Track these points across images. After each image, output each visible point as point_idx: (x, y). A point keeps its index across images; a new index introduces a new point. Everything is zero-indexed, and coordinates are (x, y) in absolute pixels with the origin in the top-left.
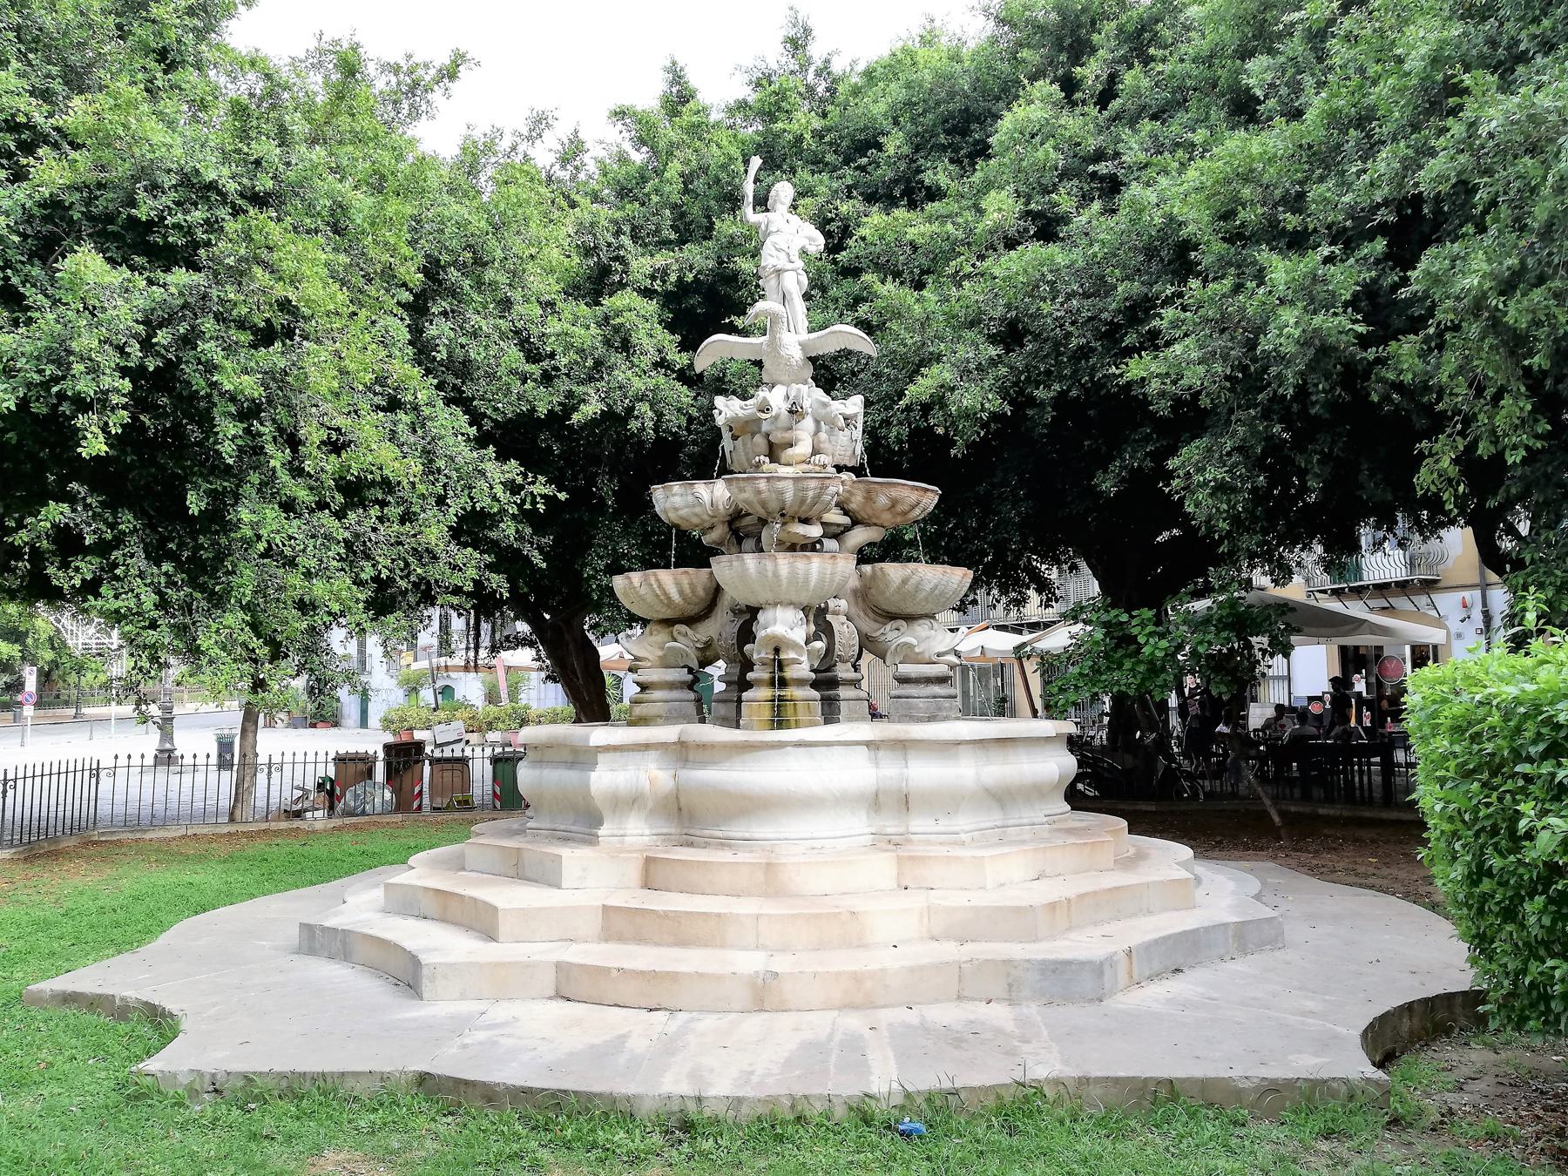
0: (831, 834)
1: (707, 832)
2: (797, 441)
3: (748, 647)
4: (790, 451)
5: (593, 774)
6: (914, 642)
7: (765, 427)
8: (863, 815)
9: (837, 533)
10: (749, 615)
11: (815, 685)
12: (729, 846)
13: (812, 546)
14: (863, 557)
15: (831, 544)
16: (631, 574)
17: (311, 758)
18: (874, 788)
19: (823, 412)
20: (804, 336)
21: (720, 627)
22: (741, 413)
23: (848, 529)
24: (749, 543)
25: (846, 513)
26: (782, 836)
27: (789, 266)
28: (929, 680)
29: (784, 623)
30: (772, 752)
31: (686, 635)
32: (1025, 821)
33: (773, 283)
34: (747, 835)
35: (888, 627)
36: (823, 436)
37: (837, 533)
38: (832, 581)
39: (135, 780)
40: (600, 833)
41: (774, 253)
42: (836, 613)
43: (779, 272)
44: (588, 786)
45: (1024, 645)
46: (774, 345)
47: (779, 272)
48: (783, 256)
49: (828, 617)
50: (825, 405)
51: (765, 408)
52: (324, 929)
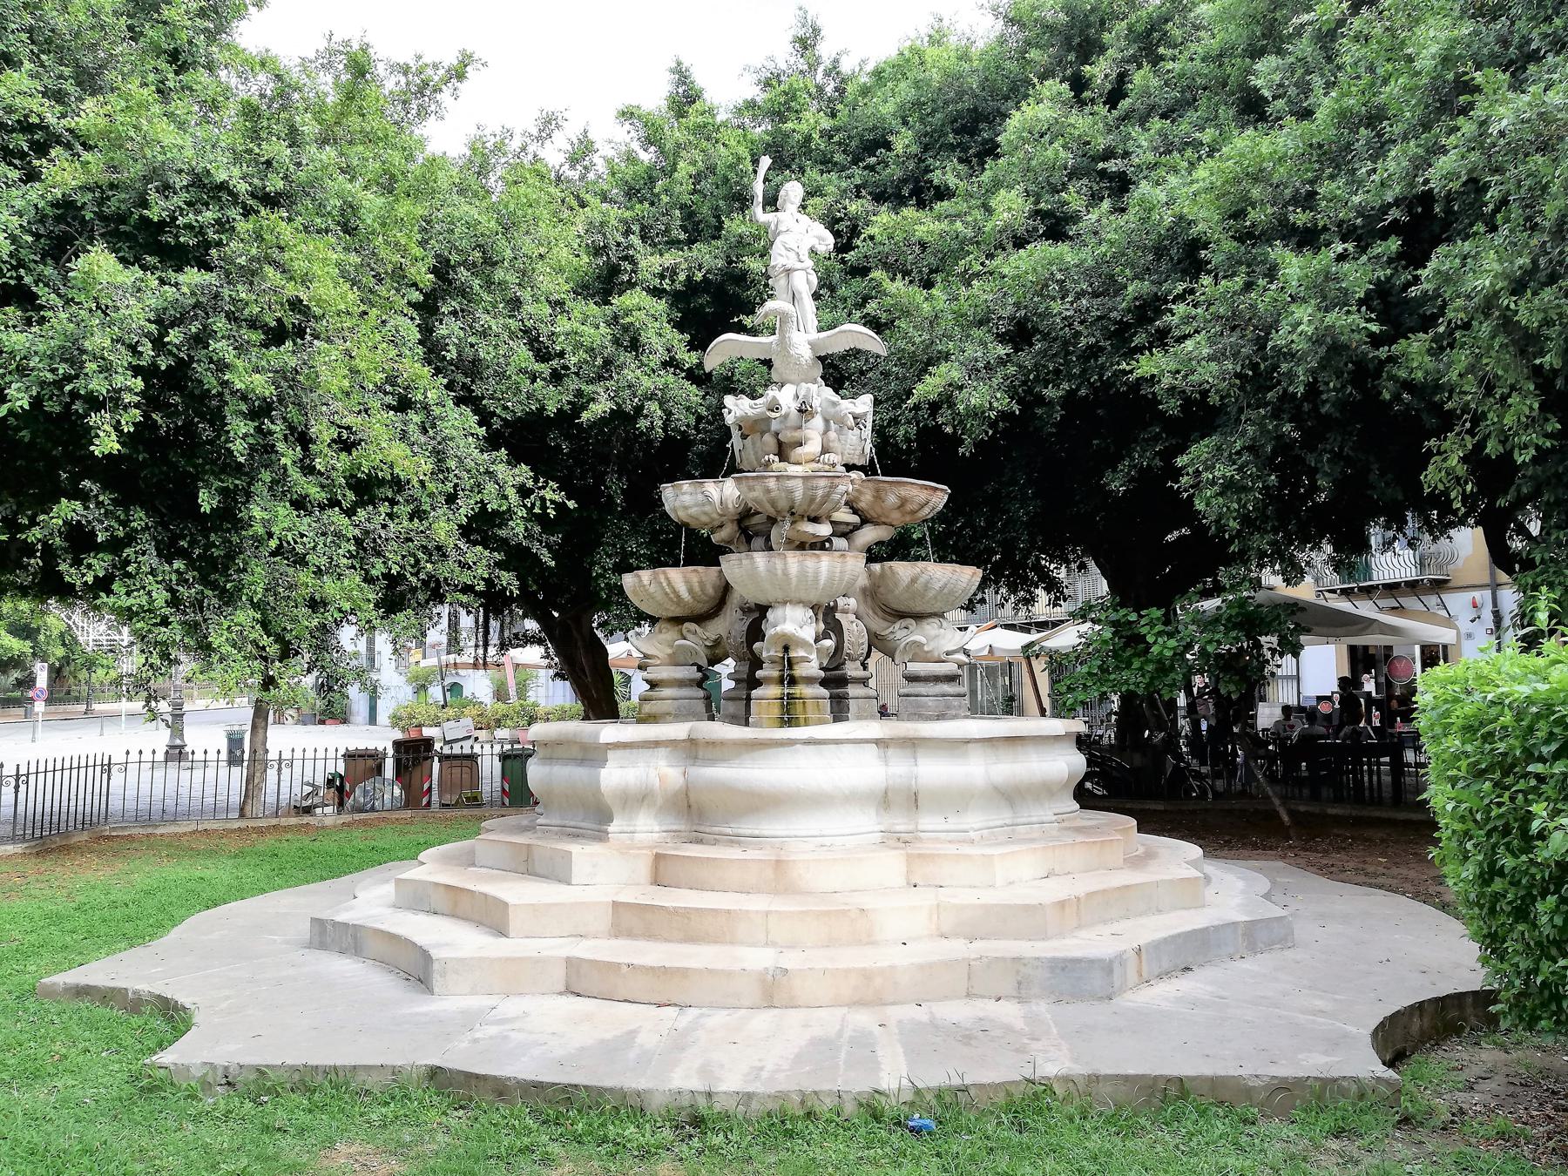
3: (757, 645)
4: (799, 450)
5: (604, 772)
6: (923, 640)
7: (774, 426)
8: (872, 812)
9: (846, 532)
12: (739, 843)
13: (821, 545)
15: (840, 543)
19: (832, 410)
20: (814, 335)
22: (750, 412)
23: (857, 528)
24: (758, 542)
25: (855, 512)
27: (799, 265)
28: (937, 679)
29: (793, 621)
32: (1034, 819)
33: (783, 282)
34: (757, 832)
35: (897, 626)
36: (832, 435)
37: (846, 532)
38: (841, 580)
39: (146, 775)
40: (610, 829)
41: (784, 252)
42: (845, 612)
43: (788, 272)
46: (784, 344)
47: (788, 272)
49: (838, 616)
50: (834, 404)
51: (775, 407)
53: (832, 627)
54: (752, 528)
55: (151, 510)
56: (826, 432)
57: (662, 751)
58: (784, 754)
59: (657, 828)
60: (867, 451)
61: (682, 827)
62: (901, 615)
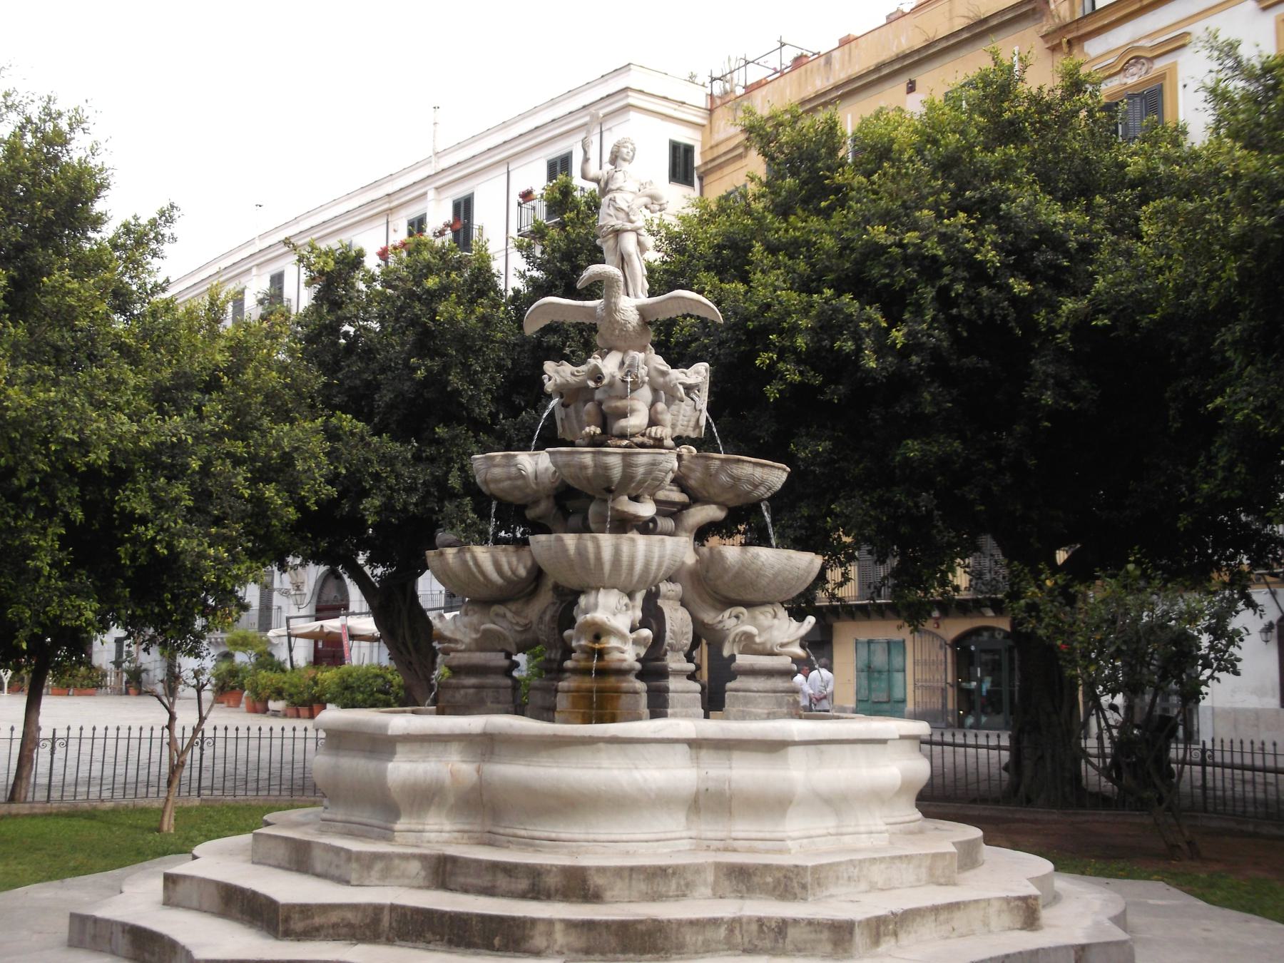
0: (761, 835)
1: (509, 831)
2: (633, 411)
3: (568, 633)
4: (623, 422)
5: (390, 765)
6: (753, 630)
7: (598, 395)
8: (682, 817)
9: (672, 511)
10: (568, 598)
11: (641, 676)
12: (532, 845)
13: (646, 527)
14: (702, 534)
15: (668, 524)
16: (600, 536)
17: (135, 733)
18: (695, 789)
19: (661, 380)
20: (644, 299)
21: (541, 607)
22: (571, 379)
23: (684, 507)
24: (575, 520)
25: (683, 489)
26: (591, 837)
27: (629, 226)
28: (770, 673)
29: (606, 608)
30: (581, 748)
31: (504, 616)
32: (862, 829)
33: (611, 242)
34: (553, 835)
35: (727, 614)
36: (661, 406)
37: (672, 511)
38: (660, 565)
39: (231, 747)
40: (398, 826)
41: (612, 211)
42: (667, 598)
43: (617, 233)
44: (385, 777)
45: (977, 632)
46: (611, 309)
47: (617, 233)
48: (622, 215)
49: (660, 602)
50: (664, 374)
51: (597, 376)
52: (96, 921)
53: (652, 616)
54: (573, 503)
55: (908, 438)
56: (653, 404)
57: (455, 747)
58: (585, 753)
59: (448, 827)
60: (703, 422)
61: (477, 828)
62: (727, 603)
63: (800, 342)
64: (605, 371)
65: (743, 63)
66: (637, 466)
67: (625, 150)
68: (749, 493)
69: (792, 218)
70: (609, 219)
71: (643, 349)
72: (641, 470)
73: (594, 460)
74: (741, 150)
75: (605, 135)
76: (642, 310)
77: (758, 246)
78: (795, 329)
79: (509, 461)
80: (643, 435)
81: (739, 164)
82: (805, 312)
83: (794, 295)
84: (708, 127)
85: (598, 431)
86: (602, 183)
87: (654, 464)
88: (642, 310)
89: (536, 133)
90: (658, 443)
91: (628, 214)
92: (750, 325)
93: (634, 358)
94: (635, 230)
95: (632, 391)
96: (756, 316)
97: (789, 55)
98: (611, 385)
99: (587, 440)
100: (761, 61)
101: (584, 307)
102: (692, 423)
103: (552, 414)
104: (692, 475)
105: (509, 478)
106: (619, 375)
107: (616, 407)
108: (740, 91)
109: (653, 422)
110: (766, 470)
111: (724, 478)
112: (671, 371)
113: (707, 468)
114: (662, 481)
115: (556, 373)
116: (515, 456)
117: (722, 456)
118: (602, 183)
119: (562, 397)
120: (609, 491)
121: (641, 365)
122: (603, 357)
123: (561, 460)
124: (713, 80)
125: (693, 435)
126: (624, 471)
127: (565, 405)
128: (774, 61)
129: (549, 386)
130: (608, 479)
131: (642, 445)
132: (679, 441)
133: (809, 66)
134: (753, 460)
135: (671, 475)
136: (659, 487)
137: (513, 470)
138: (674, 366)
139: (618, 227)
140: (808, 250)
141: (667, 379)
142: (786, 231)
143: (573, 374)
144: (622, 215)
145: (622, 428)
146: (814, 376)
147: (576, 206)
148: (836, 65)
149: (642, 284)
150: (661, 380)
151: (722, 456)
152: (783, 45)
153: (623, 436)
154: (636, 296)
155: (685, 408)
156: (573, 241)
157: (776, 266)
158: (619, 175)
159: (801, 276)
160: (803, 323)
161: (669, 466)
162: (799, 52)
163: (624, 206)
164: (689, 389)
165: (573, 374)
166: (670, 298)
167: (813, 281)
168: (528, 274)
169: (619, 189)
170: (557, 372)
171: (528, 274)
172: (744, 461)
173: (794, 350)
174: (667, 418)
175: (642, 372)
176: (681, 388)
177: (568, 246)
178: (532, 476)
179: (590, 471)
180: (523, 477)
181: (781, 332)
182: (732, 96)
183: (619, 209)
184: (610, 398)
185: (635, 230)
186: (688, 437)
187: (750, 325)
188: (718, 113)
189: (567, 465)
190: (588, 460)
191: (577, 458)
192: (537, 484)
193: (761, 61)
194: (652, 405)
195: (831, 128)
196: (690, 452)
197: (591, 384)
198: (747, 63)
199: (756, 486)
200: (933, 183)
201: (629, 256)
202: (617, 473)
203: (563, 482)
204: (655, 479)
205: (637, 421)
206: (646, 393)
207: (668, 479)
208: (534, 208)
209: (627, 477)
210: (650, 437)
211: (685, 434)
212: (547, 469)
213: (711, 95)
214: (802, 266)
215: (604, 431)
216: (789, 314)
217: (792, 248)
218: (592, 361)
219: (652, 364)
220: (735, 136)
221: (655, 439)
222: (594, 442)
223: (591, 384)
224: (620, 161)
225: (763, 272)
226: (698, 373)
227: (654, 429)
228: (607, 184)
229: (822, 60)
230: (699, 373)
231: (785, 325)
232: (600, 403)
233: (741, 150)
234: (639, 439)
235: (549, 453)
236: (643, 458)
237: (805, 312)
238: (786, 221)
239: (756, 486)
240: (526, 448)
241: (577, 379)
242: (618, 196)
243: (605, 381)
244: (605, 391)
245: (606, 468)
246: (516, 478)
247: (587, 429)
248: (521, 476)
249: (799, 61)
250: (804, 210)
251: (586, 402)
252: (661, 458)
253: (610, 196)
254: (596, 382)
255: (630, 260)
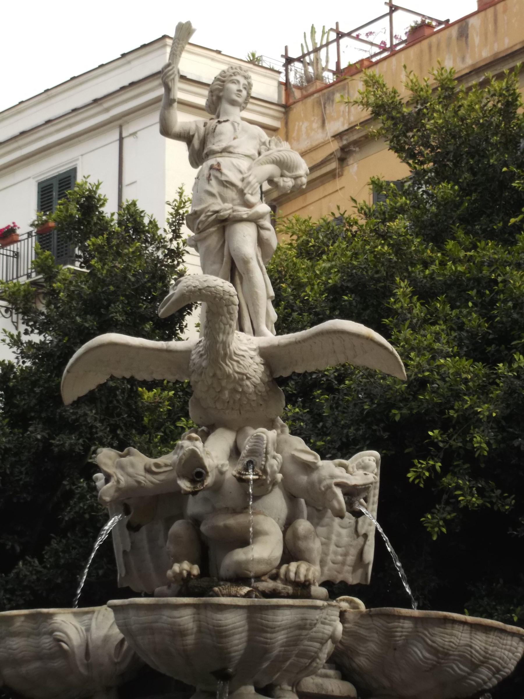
2: (258, 534)
4: (240, 555)
7: (193, 507)
19: (303, 479)
20: (269, 337)
22: (145, 479)
25: (345, 675)
27: (244, 212)
36: (303, 525)
48: (231, 194)
50: (308, 468)
63: (479, 440)
64: (208, 462)
65: (333, 36)
66: (273, 629)
67: (234, 87)
68: (463, 678)
69: (450, 245)
70: (210, 200)
71: (271, 425)
72: (281, 637)
73: (198, 621)
74: (333, 165)
75: (126, 142)
76: (267, 355)
77: (403, 287)
78: (468, 421)
79: (40, 626)
80: (275, 577)
81: (330, 187)
82: (483, 391)
83: (466, 363)
84: (283, 131)
85: (196, 570)
86: (196, 142)
87: (303, 626)
88: (267, 355)
89: (21, 142)
90: (302, 589)
91: (241, 193)
92: (396, 414)
93: (258, 438)
94: (255, 220)
95: (256, 498)
96: (406, 400)
97: (403, 24)
98: (217, 487)
99: (175, 587)
100: (362, 33)
101: (168, 351)
102: (351, 559)
103: (108, 543)
104: (362, 649)
105: (39, 657)
106: (231, 471)
107: (227, 528)
108: (329, 78)
109: (291, 553)
110: (492, 638)
111: (419, 652)
112: (321, 463)
113: (389, 635)
114: (314, 658)
115: (121, 469)
116: (50, 616)
117: (415, 612)
118: (196, 142)
119: (127, 511)
120: (223, 675)
121: (272, 452)
122: (205, 436)
123: (136, 619)
124: (289, 61)
125: (352, 580)
126: (250, 640)
127: (132, 527)
128: (380, 34)
129: (106, 491)
130: (223, 654)
131: (274, 594)
132: (335, 589)
133: (434, 39)
134: (470, 619)
135: (329, 647)
136: (307, 670)
137: (46, 641)
138: (323, 458)
139: (225, 214)
140: (480, 294)
141: (315, 476)
142: (443, 264)
143: (148, 470)
144: (231, 194)
145: (239, 564)
146: (501, 497)
147: (103, 225)
148: (475, 38)
149: (267, 313)
150: (303, 479)
151: (415, 612)
152: (393, 9)
153: (240, 578)
154: (255, 332)
155: (340, 530)
156: (102, 282)
157: (431, 319)
158: (226, 128)
159: (473, 336)
160: (483, 409)
161: (328, 630)
162: (419, 19)
163: (234, 177)
164: (352, 493)
165: (148, 470)
166: (322, 333)
167: (489, 343)
168: (25, 338)
169: (226, 151)
170: (121, 467)
171: (25, 338)
172: (454, 621)
173: (469, 454)
174: (315, 546)
175: (274, 463)
176: (339, 492)
177: (94, 289)
178: (79, 653)
179: (190, 640)
180: (64, 654)
181: (445, 426)
182: (319, 85)
183: (227, 184)
184: (216, 511)
185: (255, 220)
186: (343, 583)
187: (396, 414)
188: (298, 110)
189: (149, 630)
190: (186, 619)
191: (166, 617)
192: (88, 666)
193: (362, 33)
194: (288, 525)
195: (508, 104)
196: (355, 607)
197: (185, 485)
198: (340, 35)
199: (475, 667)
200: (50, 560)
201: (246, 262)
202: (238, 642)
203: (135, 659)
204: (303, 654)
205: (265, 550)
206: (276, 502)
207: (324, 656)
208: (17, 255)
209: (257, 648)
210: (287, 581)
211: (339, 578)
212: (106, 639)
213: (287, 84)
214: (474, 320)
215: (205, 571)
216: (457, 396)
217: (456, 290)
218: (186, 444)
219: (289, 451)
220: (325, 144)
221: (296, 584)
222: (185, 586)
223: (185, 485)
224: (225, 106)
225: (412, 327)
226: (364, 467)
227: (293, 566)
228: (204, 142)
229: (454, 31)
230: (364, 467)
231: (452, 413)
232: (196, 522)
233: (333, 165)
234: (268, 585)
235: (115, 608)
236: (285, 615)
237: (483, 391)
238: (441, 249)
239: (475, 667)
240: (68, 604)
241: (155, 479)
242: (224, 161)
243: (209, 481)
244: (206, 500)
245: (220, 634)
246: (51, 657)
247: (176, 567)
248: (60, 650)
249: (420, 32)
250: (467, 233)
251: (169, 522)
252: (316, 615)
253: (212, 161)
254: (193, 481)
255: (248, 271)
